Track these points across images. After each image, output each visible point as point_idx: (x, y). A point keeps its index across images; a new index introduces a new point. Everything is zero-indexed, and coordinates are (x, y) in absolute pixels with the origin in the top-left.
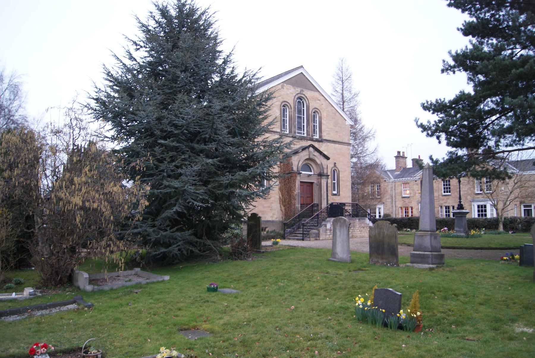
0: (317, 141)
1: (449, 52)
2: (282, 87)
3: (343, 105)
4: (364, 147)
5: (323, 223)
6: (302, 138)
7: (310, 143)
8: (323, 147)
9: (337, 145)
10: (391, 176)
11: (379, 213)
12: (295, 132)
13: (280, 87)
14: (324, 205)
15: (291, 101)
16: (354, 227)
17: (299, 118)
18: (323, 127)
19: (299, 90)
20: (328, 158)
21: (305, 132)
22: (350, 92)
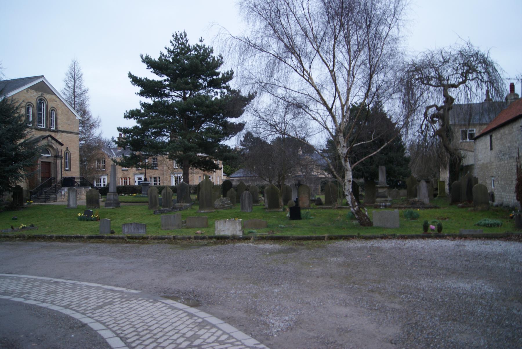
0: (54, 131)
1: (125, 117)
2: (27, 91)
3: (74, 98)
4: (90, 133)
5: (59, 191)
6: (42, 130)
7: (48, 133)
8: (58, 136)
9: (69, 134)
10: (114, 153)
11: (104, 182)
12: (37, 125)
13: (25, 91)
14: (59, 178)
15: (34, 102)
16: (81, 193)
17: (40, 114)
18: (59, 121)
19: (40, 93)
20: (62, 145)
21: (45, 125)
22: (80, 89)
